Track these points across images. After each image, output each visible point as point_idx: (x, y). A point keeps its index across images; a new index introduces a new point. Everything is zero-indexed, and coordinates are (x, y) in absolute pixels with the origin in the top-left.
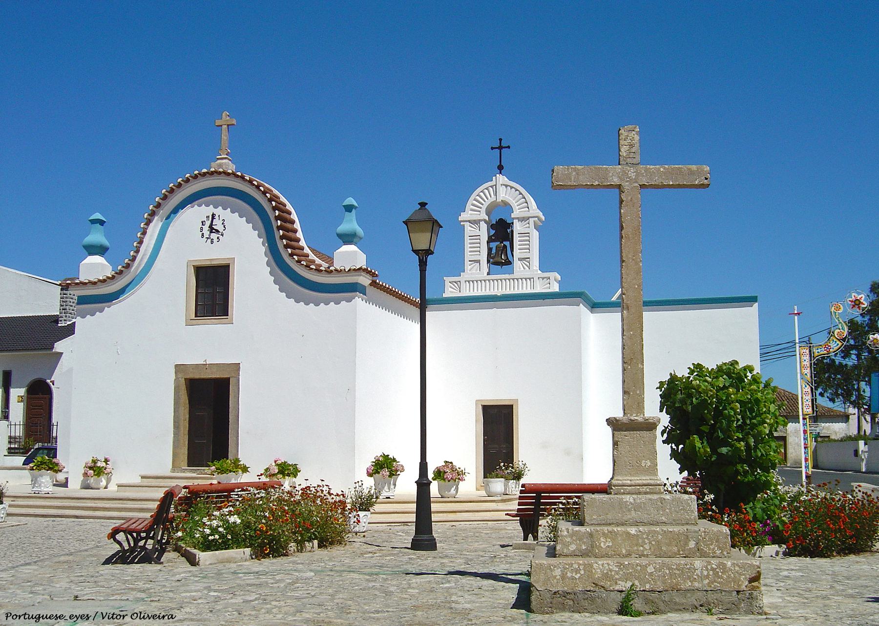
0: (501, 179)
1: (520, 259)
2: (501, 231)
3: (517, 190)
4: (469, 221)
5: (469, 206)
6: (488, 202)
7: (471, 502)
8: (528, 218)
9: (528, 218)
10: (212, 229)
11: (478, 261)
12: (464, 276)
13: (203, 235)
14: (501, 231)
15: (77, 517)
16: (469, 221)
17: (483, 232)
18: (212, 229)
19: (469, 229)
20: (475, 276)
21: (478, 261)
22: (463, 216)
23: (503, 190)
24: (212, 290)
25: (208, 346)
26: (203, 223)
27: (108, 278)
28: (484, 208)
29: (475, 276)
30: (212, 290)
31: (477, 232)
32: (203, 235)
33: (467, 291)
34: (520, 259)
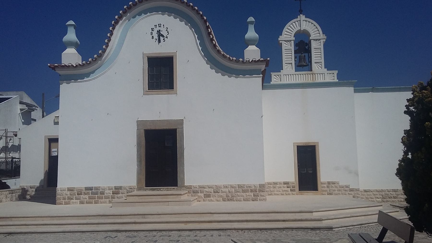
0: (302, 17)
1: (315, 63)
2: (303, 46)
3: (312, 23)
4: (285, 41)
5: (284, 32)
6: (295, 31)
7: (130, 215)
8: (320, 40)
9: (320, 40)
10: (160, 35)
11: (291, 64)
12: (283, 72)
13: (153, 37)
14: (303, 46)
15: (292, 229)
16: (285, 41)
17: (292, 47)
18: (160, 35)
19: (285, 46)
20: (288, 72)
21: (291, 64)
22: (281, 38)
23: (304, 24)
24: (161, 73)
25: (160, 109)
26: (152, 29)
27: (72, 66)
28: (293, 35)
29: (288, 72)
30: (161, 73)
31: (289, 47)
32: (153, 37)
33: (285, 81)
34: (315, 63)
